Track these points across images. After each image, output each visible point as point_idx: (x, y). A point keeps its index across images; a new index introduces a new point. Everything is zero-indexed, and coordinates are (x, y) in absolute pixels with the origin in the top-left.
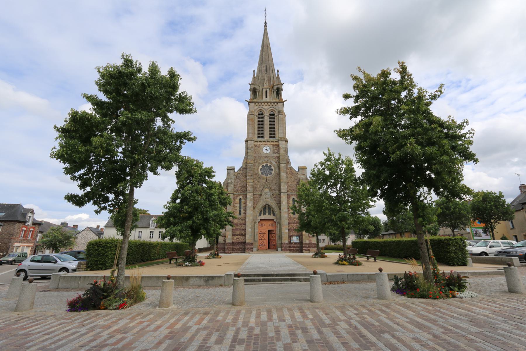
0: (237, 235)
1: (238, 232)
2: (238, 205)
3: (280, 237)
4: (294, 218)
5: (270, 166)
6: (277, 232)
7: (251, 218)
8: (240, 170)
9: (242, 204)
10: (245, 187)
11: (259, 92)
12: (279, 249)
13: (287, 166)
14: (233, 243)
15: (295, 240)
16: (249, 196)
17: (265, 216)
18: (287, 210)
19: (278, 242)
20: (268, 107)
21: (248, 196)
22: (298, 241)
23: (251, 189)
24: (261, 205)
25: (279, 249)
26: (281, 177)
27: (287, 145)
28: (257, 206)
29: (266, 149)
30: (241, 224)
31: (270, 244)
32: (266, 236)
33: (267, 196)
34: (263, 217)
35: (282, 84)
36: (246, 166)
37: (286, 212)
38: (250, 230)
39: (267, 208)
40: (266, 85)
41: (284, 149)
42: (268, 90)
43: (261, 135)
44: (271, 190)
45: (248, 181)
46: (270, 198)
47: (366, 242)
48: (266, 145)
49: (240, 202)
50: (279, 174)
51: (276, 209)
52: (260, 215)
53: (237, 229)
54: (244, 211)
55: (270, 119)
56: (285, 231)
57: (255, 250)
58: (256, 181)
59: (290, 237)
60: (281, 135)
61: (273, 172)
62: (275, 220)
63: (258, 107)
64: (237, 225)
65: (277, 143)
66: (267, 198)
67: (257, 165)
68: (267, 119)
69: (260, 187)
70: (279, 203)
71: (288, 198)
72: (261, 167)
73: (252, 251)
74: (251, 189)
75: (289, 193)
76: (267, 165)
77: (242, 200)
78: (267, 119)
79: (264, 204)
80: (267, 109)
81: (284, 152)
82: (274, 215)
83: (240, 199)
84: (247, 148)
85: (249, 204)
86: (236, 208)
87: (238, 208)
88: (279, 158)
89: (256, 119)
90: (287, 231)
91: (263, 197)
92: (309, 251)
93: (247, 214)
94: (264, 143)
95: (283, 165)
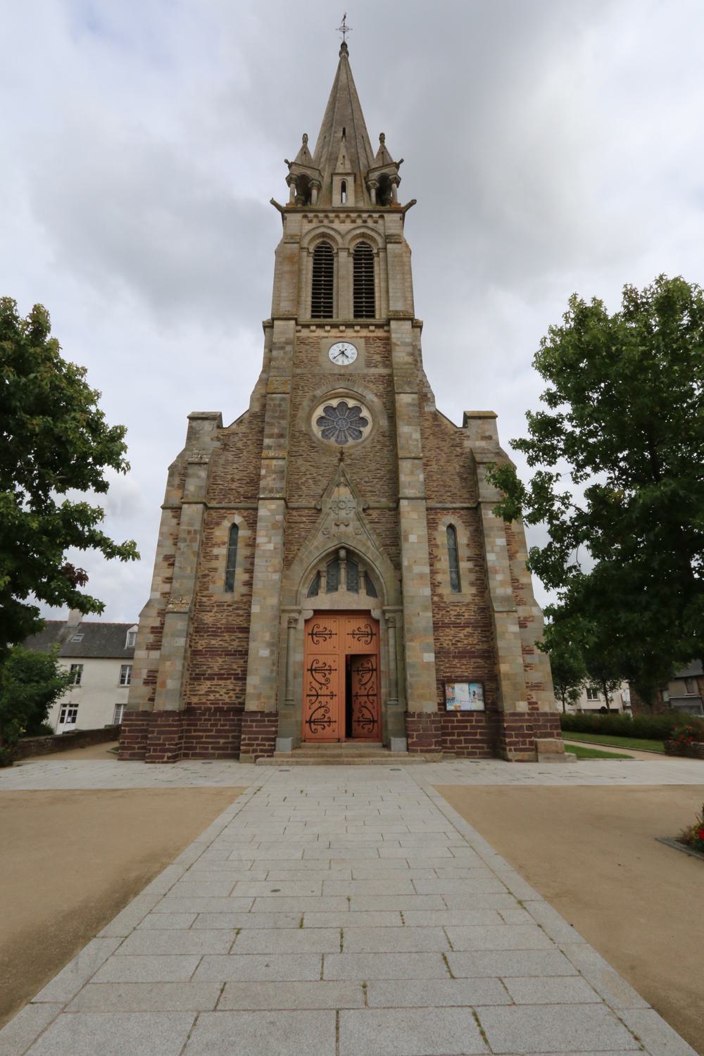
0: (211, 678)
1: (216, 664)
2: (222, 551)
3: (401, 688)
4: (455, 604)
5: (358, 409)
6: (387, 664)
7: (273, 601)
8: (240, 421)
9: (240, 545)
10: (255, 481)
11: (319, 188)
12: (398, 743)
13: (420, 407)
14: (189, 711)
15: (465, 697)
16: (269, 511)
17: (335, 595)
18: (427, 570)
19: (392, 709)
20: (348, 226)
21: (262, 512)
22: (479, 705)
23: (278, 485)
24: (316, 547)
25: (398, 743)
26: (401, 442)
27: (417, 338)
28: (303, 554)
29: (343, 352)
30: (230, 629)
31: (356, 715)
32: (337, 682)
33: (343, 513)
34: (324, 601)
35: (397, 166)
36: (264, 406)
37: (421, 576)
38: (265, 653)
39: (344, 561)
40: (344, 166)
41: (410, 349)
42: (350, 180)
43: (322, 306)
44: (357, 492)
45: (265, 453)
46: (354, 524)
47: (456, 739)
48: (341, 339)
49: (233, 541)
50: (391, 436)
51: (381, 567)
52: (314, 592)
53: (212, 652)
54: (246, 577)
55: (357, 266)
56: (422, 656)
57: (284, 744)
58: (300, 461)
59: (444, 683)
60: (397, 306)
61: (366, 431)
62: (376, 614)
63: (313, 225)
64: (215, 634)
65: (380, 333)
66: (344, 520)
67: (306, 403)
68: (344, 267)
69: (316, 482)
70: (394, 543)
71: (432, 525)
72: (319, 412)
73: (271, 752)
74: (278, 485)
75: (432, 504)
76: (343, 404)
77: (241, 533)
78: (344, 267)
79: (331, 545)
80: (344, 232)
81: (410, 359)
82: (371, 592)
83: (234, 527)
84: (270, 347)
85: (268, 543)
86: (214, 564)
87: (221, 565)
88: (389, 381)
89: (308, 264)
90: (430, 657)
91: (327, 520)
92: (535, 748)
93: (258, 585)
94: (334, 332)
95: (404, 399)
